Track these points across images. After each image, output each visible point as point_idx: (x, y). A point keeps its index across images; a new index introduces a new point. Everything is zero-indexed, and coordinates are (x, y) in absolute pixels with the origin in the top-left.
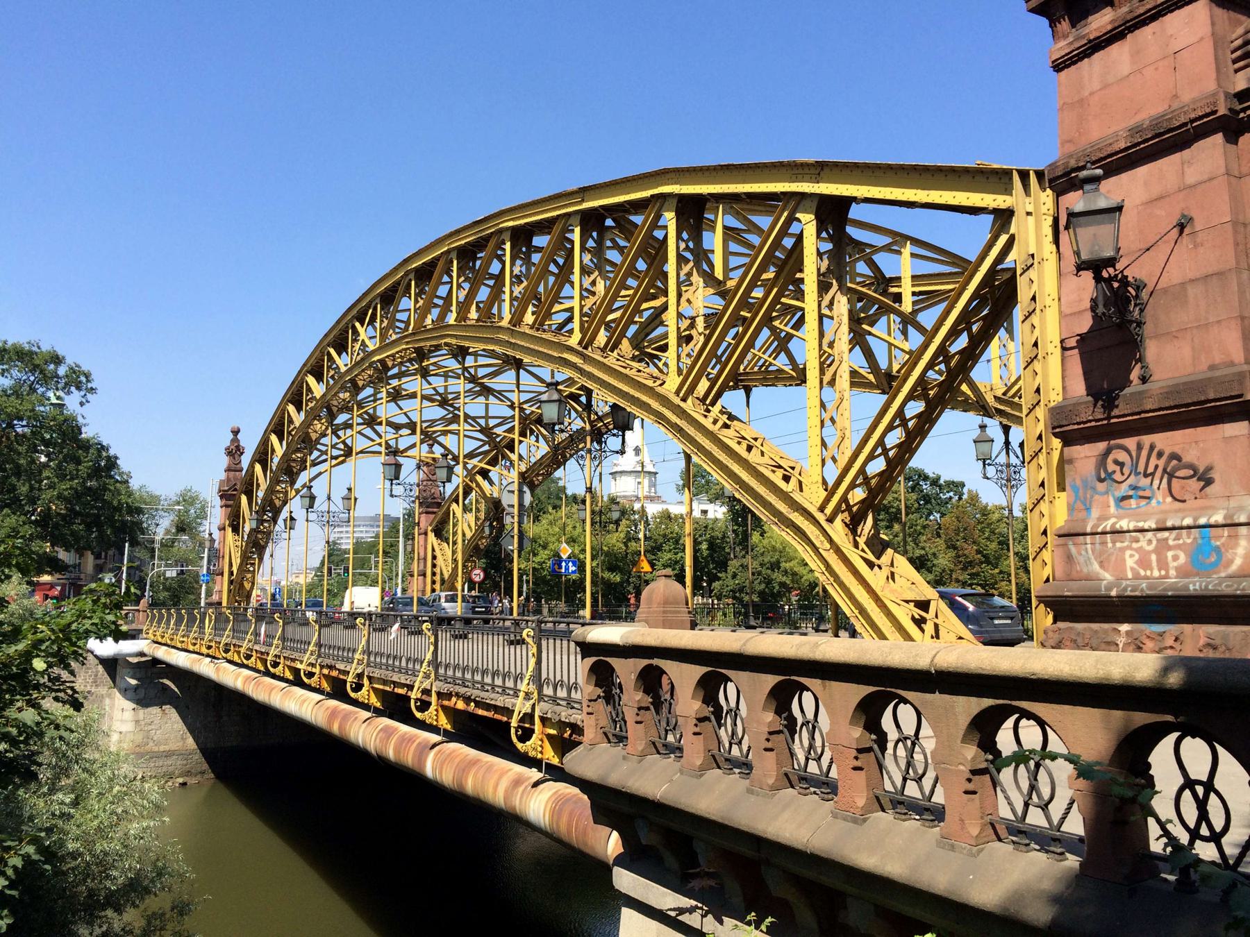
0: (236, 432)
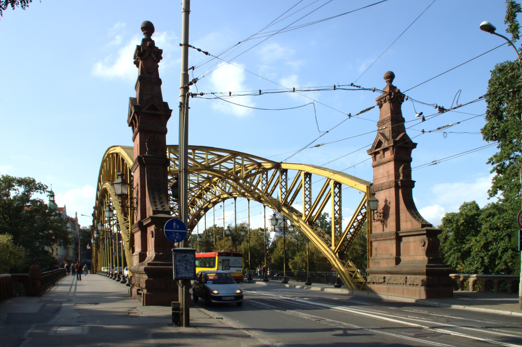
0: (391, 77)
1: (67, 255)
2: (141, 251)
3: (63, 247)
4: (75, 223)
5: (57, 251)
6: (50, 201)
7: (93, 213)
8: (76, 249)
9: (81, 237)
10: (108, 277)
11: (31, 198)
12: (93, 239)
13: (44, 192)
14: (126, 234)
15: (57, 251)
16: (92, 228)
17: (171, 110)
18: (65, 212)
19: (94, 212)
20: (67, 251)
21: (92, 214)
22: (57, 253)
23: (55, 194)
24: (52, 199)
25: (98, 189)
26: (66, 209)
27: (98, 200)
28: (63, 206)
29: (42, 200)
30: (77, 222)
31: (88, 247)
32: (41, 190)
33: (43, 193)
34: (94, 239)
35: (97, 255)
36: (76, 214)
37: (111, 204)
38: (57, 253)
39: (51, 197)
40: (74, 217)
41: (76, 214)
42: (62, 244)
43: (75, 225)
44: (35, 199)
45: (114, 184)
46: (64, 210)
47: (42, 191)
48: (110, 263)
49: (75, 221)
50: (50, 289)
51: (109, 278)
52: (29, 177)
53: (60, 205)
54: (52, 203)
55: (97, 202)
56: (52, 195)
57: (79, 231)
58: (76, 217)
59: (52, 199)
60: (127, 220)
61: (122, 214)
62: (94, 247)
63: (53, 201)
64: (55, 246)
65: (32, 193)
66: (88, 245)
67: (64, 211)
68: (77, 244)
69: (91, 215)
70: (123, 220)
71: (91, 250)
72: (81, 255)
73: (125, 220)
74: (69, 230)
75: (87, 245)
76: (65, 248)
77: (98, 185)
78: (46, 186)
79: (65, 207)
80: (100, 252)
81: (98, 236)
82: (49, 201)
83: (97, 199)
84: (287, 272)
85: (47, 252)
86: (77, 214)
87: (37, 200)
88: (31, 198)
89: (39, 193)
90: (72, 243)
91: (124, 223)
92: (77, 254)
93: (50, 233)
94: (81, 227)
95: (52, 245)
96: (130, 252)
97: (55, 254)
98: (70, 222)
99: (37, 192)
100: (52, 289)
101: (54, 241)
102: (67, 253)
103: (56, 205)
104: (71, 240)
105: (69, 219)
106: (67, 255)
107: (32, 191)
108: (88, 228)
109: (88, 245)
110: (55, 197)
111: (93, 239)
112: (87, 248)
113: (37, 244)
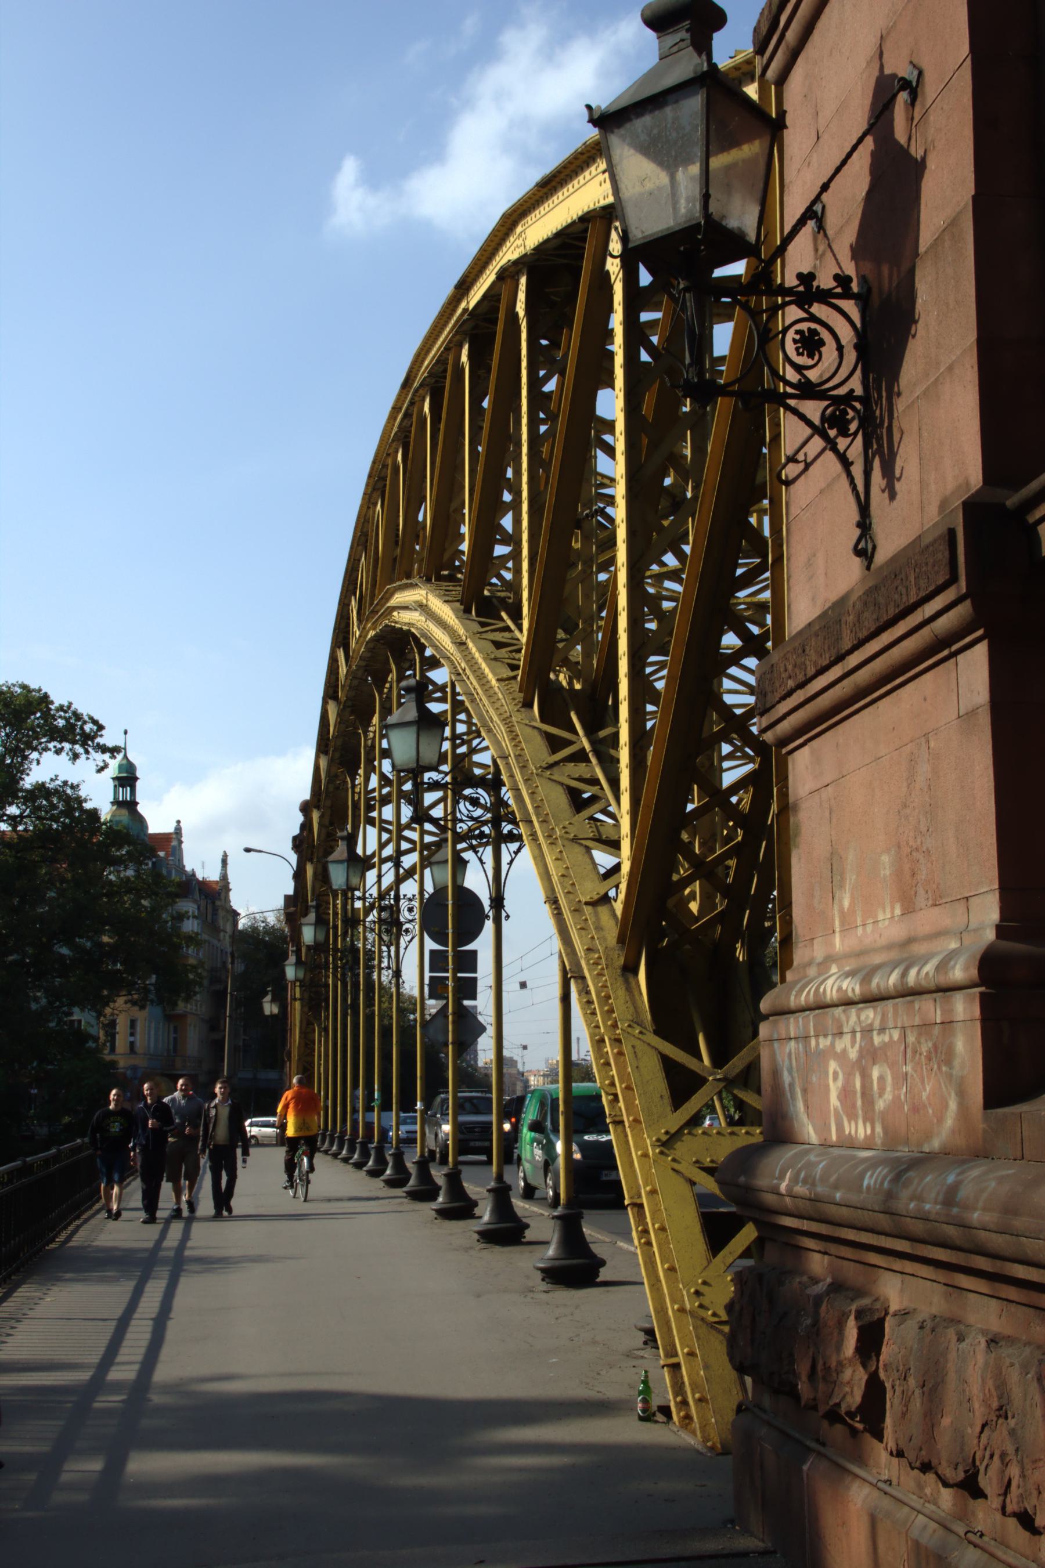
0: (179, 822)
1: (175, 1050)
2: (1001, 931)
3: (158, 1010)
4: (218, 903)
5: (132, 1034)
6: (116, 802)
7: (296, 831)
8: (214, 1024)
9: (240, 967)
10: (346, 1160)
11: (28, 782)
12: (292, 959)
13: (87, 752)
14: (575, 840)
15: (132, 1034)
16: (292, 909)
17: (589, 122)
18: (177, 852)
19: (306, 826)
20: (176, 1031)
21: (295, 839)
22: (132, 1044)
23: (138, 774)
24: (124, 794)
25: (341, 636)
26: (183, 839)
27: (326, 753)
28: (170, 829)
29: (72, 787)
30: (227, 900)
31: (270, 1008)
32: (74, 742)
33: (83, 756)
34: (299, 963)
35: (307, 1044)
36: (224, 862)
37: (440, 676)
38: (132, 1044)
39: (123, 786)
40: (210, 873)
41: (224, 862)
42: (151, 996)
43: (215, 911)
44: (43, 784)
45: (387, 727)
46: (174, 843)
47: (78, 749)
48: (355, 1086)
49: (219, 894)
50: (69, 1238)
51: (349, 1168)
52: (24, 687)
53: (157, 823)
54: (124, 812)
55: (323, 763)
56: (127, 779)
57: (232, 936)
58: (224, 877)
59: (124, 794)
60: (570, 743)
61: (528, 704)
62: (298, 1004)
63: (130, 806)
64: (120, 1007)
65: (35, 755)
66: (269, 998)
67: (174, 848)
68: (218, 998)
69: (289, 844)
70: (539, 741)
71: (282, 1019)
72: (234, 1049)
73: (554, 744)
74: (190, 926)
75: (266, 994)
76: (169, 1018)
77: (333, 661)
78: (95, 722)
79: (178, 831)
80: (326, 1030)
81: (321, 937)
82: (113, 803)
83: (331, 691)
84: (486, 1092)
85: (80, 1037)
86: (229, 861)
87: (51, 786)
88: (28, 782)
89: (64, 757)
90: (197, 989)
91: (551, 766)
92: (219, 1045)
93: (102, 945)
94: (242, 923)
95: (107, 1001)
96: (631, 989)
97: (121, 1042)
98: (197, 896)
99: (58, 752)
100: (78, 1239)
101: (117, 984)
102: (175, 1039)
103: (140, 821)
104: (191, 976)
105: (190, 886)
106: (175, 1050)
107: (35, 749)
108: (271, 920)
109: (269, 998)
110: (138, 784)
111: (292, 959)
112: (261, 1009)
113: (36, 1000)
